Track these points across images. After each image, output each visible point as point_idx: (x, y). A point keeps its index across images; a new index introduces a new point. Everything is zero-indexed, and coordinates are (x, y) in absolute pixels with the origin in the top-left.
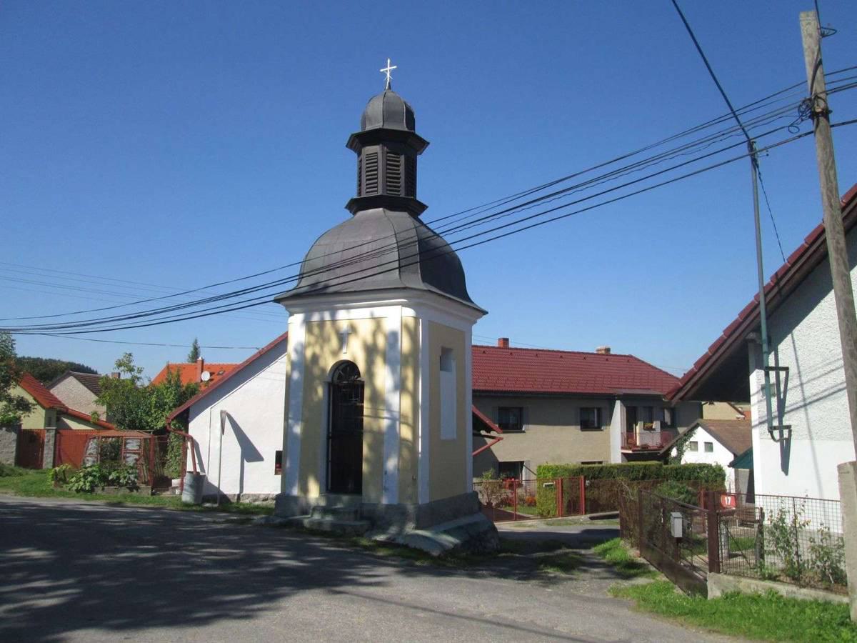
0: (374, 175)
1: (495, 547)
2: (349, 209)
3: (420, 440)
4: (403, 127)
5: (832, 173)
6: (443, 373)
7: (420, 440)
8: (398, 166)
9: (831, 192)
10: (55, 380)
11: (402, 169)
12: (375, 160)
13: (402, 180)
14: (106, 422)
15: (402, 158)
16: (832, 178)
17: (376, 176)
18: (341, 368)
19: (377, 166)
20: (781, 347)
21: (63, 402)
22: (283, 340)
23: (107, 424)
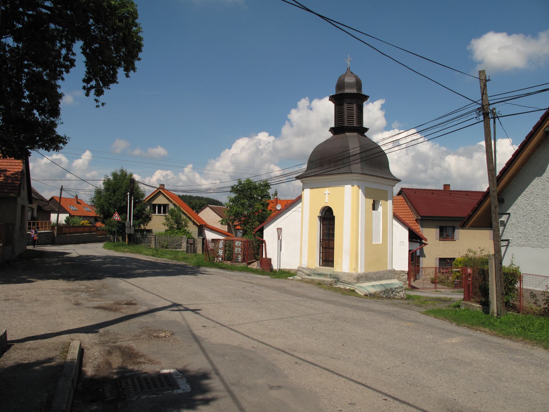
0: (341, 115)
1: (402, 296)
2: (331, 131)
3: (133, 200)
4: (354, 91)
5: (488, 138)
6: (373, 211)
7: (133, 200)
8: (353, 110)
9: (488, 146)
10: (410, 256)
11: (355, 112)
12: (342, 112)
13: (355, 117)
14: (227, 232)
15: (355, 106)
16: (489, 141)
17: (342, 116)
18: (325, 210)
19: (342, 115)
20: (397, 214)
21: (206, 221)
22: (321, 165)
23: (228, 233)
